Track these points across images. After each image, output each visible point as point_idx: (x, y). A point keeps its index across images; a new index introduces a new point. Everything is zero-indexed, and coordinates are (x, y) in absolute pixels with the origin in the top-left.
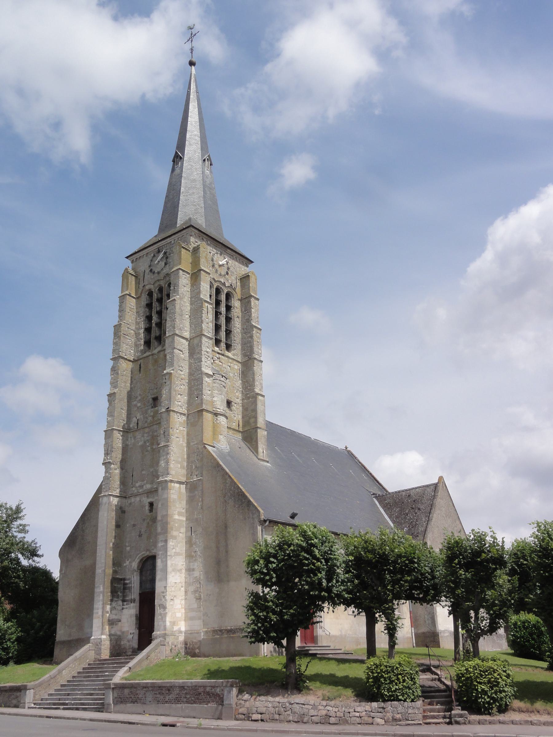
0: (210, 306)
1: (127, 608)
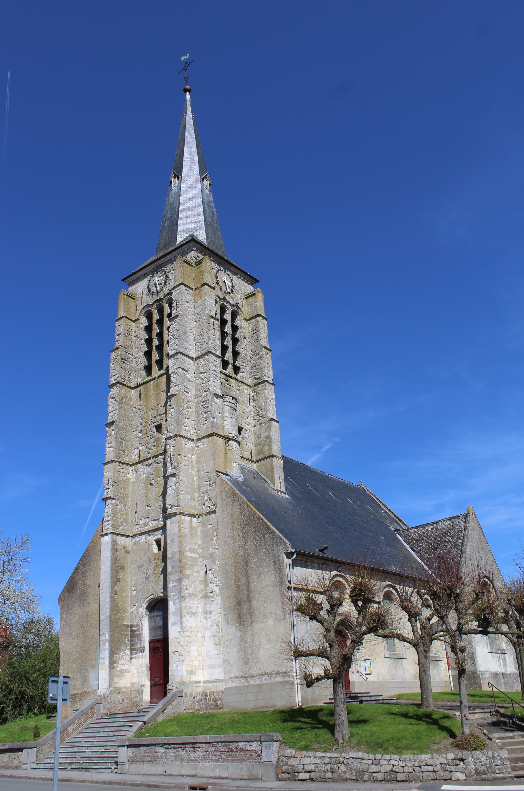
0: (216, 322)
1: (136, 658)
